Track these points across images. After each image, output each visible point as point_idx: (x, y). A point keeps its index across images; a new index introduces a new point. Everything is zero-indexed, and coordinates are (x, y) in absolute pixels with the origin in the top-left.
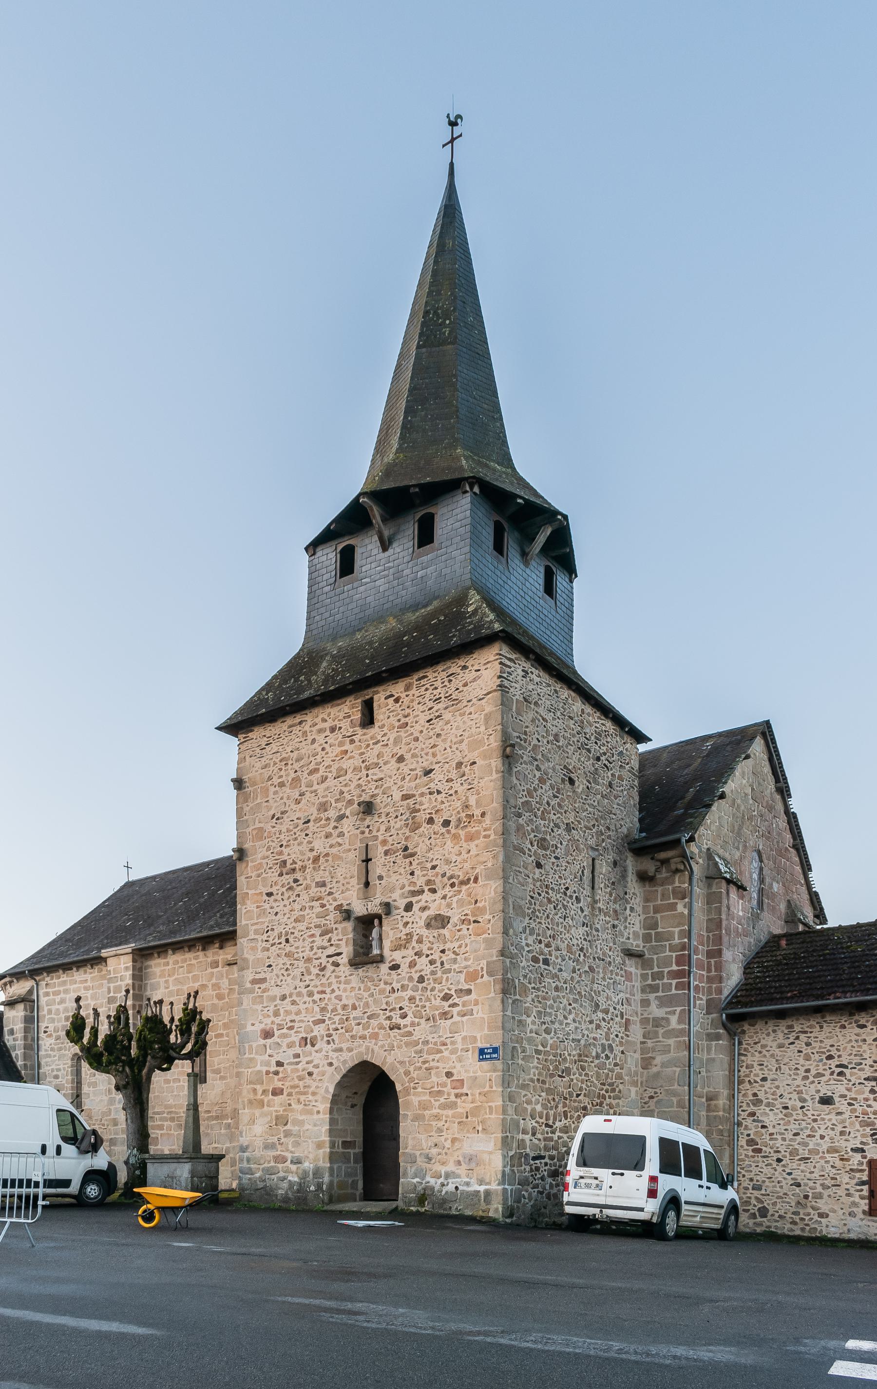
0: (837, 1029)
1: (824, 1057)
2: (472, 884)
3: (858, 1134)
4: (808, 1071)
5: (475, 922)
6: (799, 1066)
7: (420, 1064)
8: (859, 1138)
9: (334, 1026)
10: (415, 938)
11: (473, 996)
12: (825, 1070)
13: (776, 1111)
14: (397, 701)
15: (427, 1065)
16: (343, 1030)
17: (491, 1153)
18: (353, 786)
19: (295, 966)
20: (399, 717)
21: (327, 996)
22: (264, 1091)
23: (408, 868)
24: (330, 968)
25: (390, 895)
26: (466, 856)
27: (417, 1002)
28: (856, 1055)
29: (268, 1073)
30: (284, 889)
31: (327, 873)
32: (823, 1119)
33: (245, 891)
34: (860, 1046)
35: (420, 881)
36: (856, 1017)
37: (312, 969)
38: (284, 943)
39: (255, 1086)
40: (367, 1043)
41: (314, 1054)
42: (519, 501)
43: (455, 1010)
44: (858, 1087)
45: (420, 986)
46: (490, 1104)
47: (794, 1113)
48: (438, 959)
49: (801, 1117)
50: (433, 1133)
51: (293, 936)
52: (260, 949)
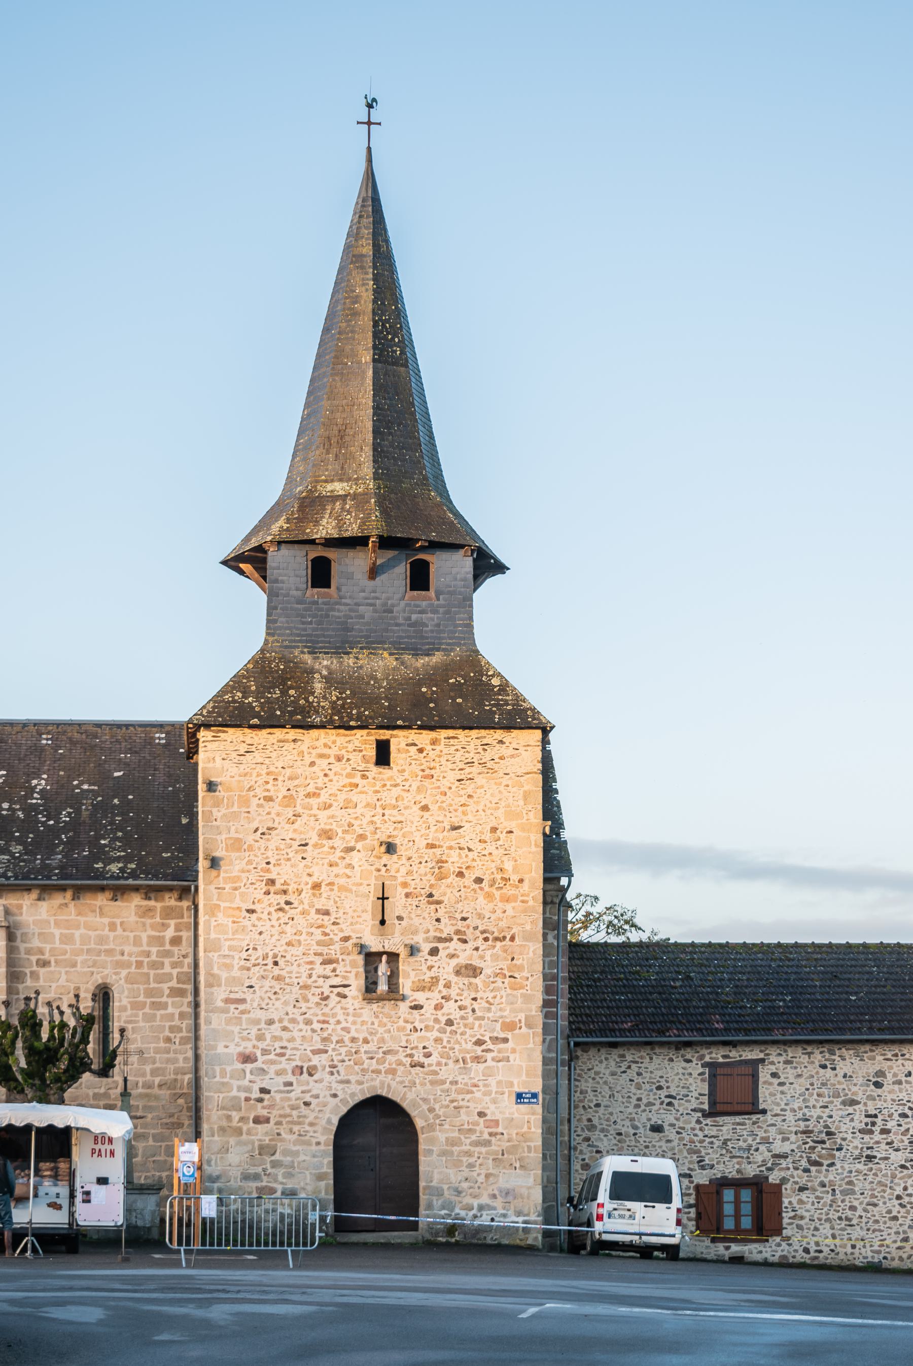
0: (666, 1062)
1: (654, 1087)
2: (507, 942)
3: (686, 1161)
4: (639, 1099)
5: (510, 977)
6: (631, 1095)
7: (447, 1102)
8: (687, 1164)
9: (340, 1058)
10: (442, 982)
11: (510, 1045)
12: (655, 1099)
13: (610, 1137)
14: (421, 751)
15: (455, 1104)
16: (352, 1063)
17: (529, 1188)
18: (365, 821)
19: (288, 991)
20: (422, 767)
21: (331, 1027)
22: (242, 1119)
23: (432, 914)
24: (334, 999)
25: (411, 936)
26: (501, 915)
27: (445, 1043)
28: (683, 1087)
29: (247, 1099)
30: (272, 909)
31: (332, 902)
32: (654, 1146)
33: (215, 902)
34: (686, 1080)
35: (447, 929)
36: (682, 1052)
37: (310, 996)
38: (271, 965)
39: (230, 1113)
40: (382, 1077)
41: (312, 1084)
42: (492, 561)
43: (489, 1056)
44: (686, 1117)
45: (449, 1029)
46: (528, 1144)
47: (627, 1139)
48: (469, 1005)
49: (633, 1143)
50: (463, 1168)
51: (283, 959)
52: (236, 967)
